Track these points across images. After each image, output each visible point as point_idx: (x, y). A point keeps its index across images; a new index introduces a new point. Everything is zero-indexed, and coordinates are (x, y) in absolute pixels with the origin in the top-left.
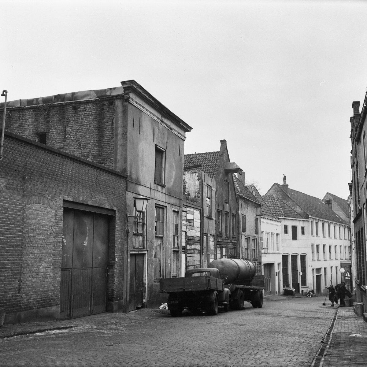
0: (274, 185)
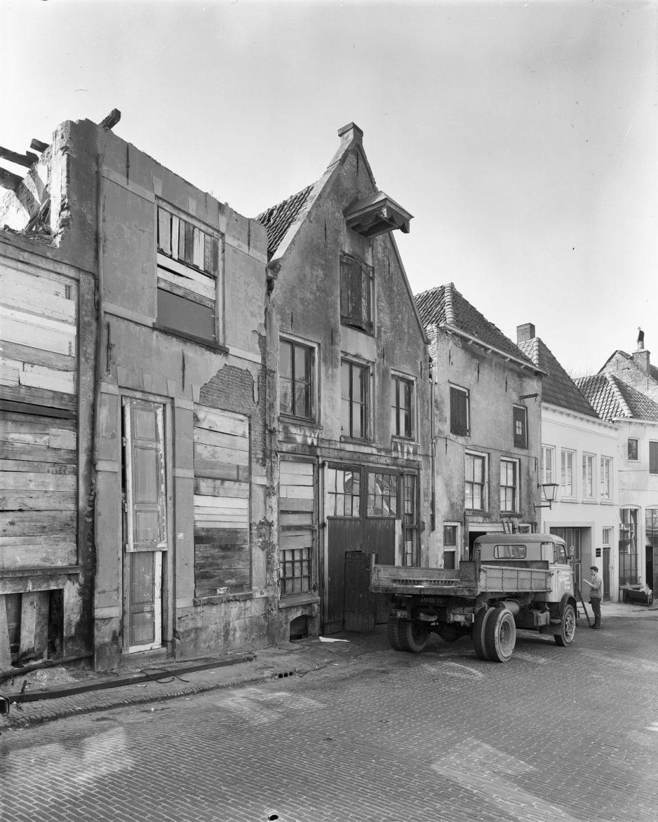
0: (614, 354)
